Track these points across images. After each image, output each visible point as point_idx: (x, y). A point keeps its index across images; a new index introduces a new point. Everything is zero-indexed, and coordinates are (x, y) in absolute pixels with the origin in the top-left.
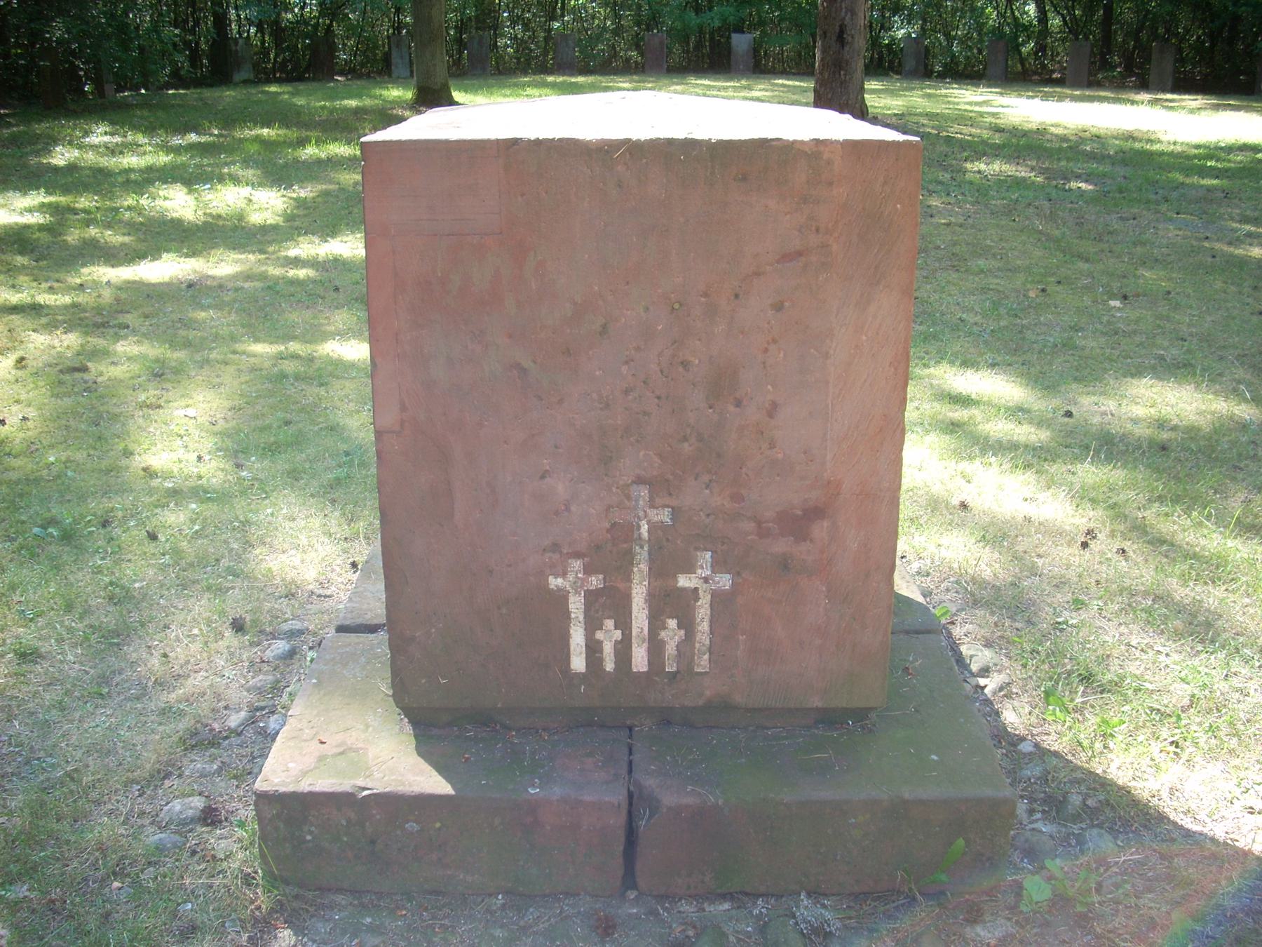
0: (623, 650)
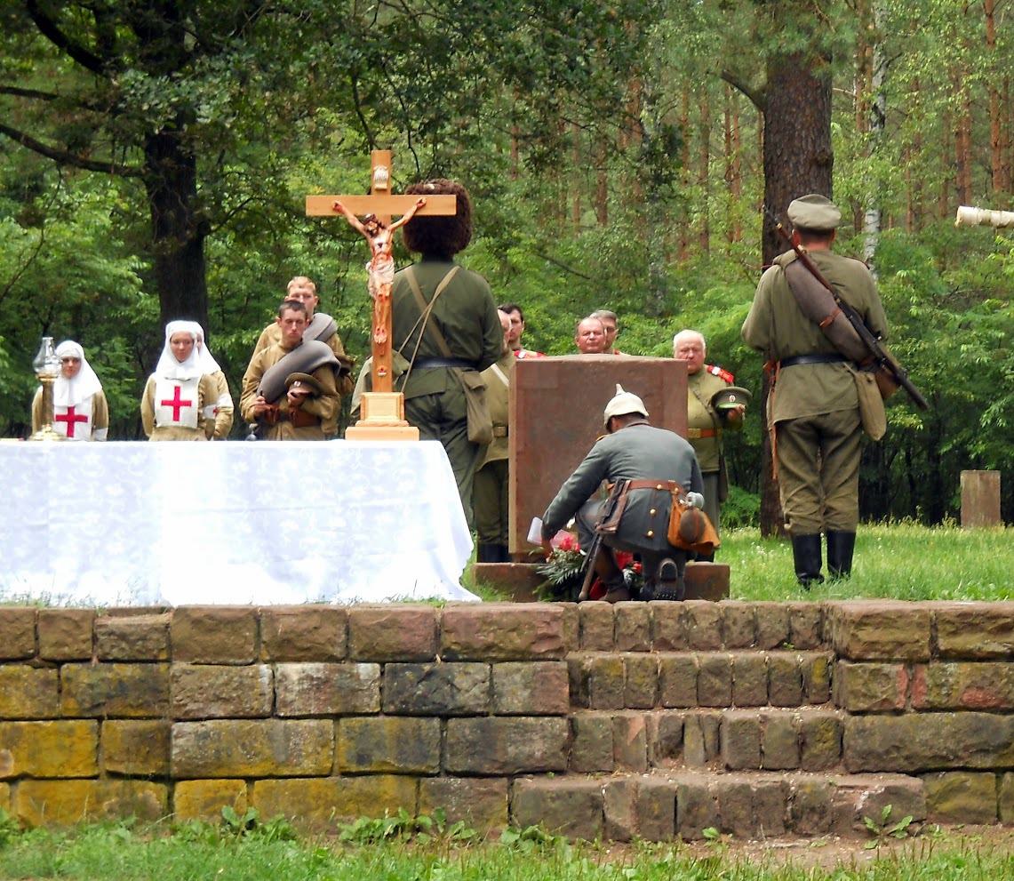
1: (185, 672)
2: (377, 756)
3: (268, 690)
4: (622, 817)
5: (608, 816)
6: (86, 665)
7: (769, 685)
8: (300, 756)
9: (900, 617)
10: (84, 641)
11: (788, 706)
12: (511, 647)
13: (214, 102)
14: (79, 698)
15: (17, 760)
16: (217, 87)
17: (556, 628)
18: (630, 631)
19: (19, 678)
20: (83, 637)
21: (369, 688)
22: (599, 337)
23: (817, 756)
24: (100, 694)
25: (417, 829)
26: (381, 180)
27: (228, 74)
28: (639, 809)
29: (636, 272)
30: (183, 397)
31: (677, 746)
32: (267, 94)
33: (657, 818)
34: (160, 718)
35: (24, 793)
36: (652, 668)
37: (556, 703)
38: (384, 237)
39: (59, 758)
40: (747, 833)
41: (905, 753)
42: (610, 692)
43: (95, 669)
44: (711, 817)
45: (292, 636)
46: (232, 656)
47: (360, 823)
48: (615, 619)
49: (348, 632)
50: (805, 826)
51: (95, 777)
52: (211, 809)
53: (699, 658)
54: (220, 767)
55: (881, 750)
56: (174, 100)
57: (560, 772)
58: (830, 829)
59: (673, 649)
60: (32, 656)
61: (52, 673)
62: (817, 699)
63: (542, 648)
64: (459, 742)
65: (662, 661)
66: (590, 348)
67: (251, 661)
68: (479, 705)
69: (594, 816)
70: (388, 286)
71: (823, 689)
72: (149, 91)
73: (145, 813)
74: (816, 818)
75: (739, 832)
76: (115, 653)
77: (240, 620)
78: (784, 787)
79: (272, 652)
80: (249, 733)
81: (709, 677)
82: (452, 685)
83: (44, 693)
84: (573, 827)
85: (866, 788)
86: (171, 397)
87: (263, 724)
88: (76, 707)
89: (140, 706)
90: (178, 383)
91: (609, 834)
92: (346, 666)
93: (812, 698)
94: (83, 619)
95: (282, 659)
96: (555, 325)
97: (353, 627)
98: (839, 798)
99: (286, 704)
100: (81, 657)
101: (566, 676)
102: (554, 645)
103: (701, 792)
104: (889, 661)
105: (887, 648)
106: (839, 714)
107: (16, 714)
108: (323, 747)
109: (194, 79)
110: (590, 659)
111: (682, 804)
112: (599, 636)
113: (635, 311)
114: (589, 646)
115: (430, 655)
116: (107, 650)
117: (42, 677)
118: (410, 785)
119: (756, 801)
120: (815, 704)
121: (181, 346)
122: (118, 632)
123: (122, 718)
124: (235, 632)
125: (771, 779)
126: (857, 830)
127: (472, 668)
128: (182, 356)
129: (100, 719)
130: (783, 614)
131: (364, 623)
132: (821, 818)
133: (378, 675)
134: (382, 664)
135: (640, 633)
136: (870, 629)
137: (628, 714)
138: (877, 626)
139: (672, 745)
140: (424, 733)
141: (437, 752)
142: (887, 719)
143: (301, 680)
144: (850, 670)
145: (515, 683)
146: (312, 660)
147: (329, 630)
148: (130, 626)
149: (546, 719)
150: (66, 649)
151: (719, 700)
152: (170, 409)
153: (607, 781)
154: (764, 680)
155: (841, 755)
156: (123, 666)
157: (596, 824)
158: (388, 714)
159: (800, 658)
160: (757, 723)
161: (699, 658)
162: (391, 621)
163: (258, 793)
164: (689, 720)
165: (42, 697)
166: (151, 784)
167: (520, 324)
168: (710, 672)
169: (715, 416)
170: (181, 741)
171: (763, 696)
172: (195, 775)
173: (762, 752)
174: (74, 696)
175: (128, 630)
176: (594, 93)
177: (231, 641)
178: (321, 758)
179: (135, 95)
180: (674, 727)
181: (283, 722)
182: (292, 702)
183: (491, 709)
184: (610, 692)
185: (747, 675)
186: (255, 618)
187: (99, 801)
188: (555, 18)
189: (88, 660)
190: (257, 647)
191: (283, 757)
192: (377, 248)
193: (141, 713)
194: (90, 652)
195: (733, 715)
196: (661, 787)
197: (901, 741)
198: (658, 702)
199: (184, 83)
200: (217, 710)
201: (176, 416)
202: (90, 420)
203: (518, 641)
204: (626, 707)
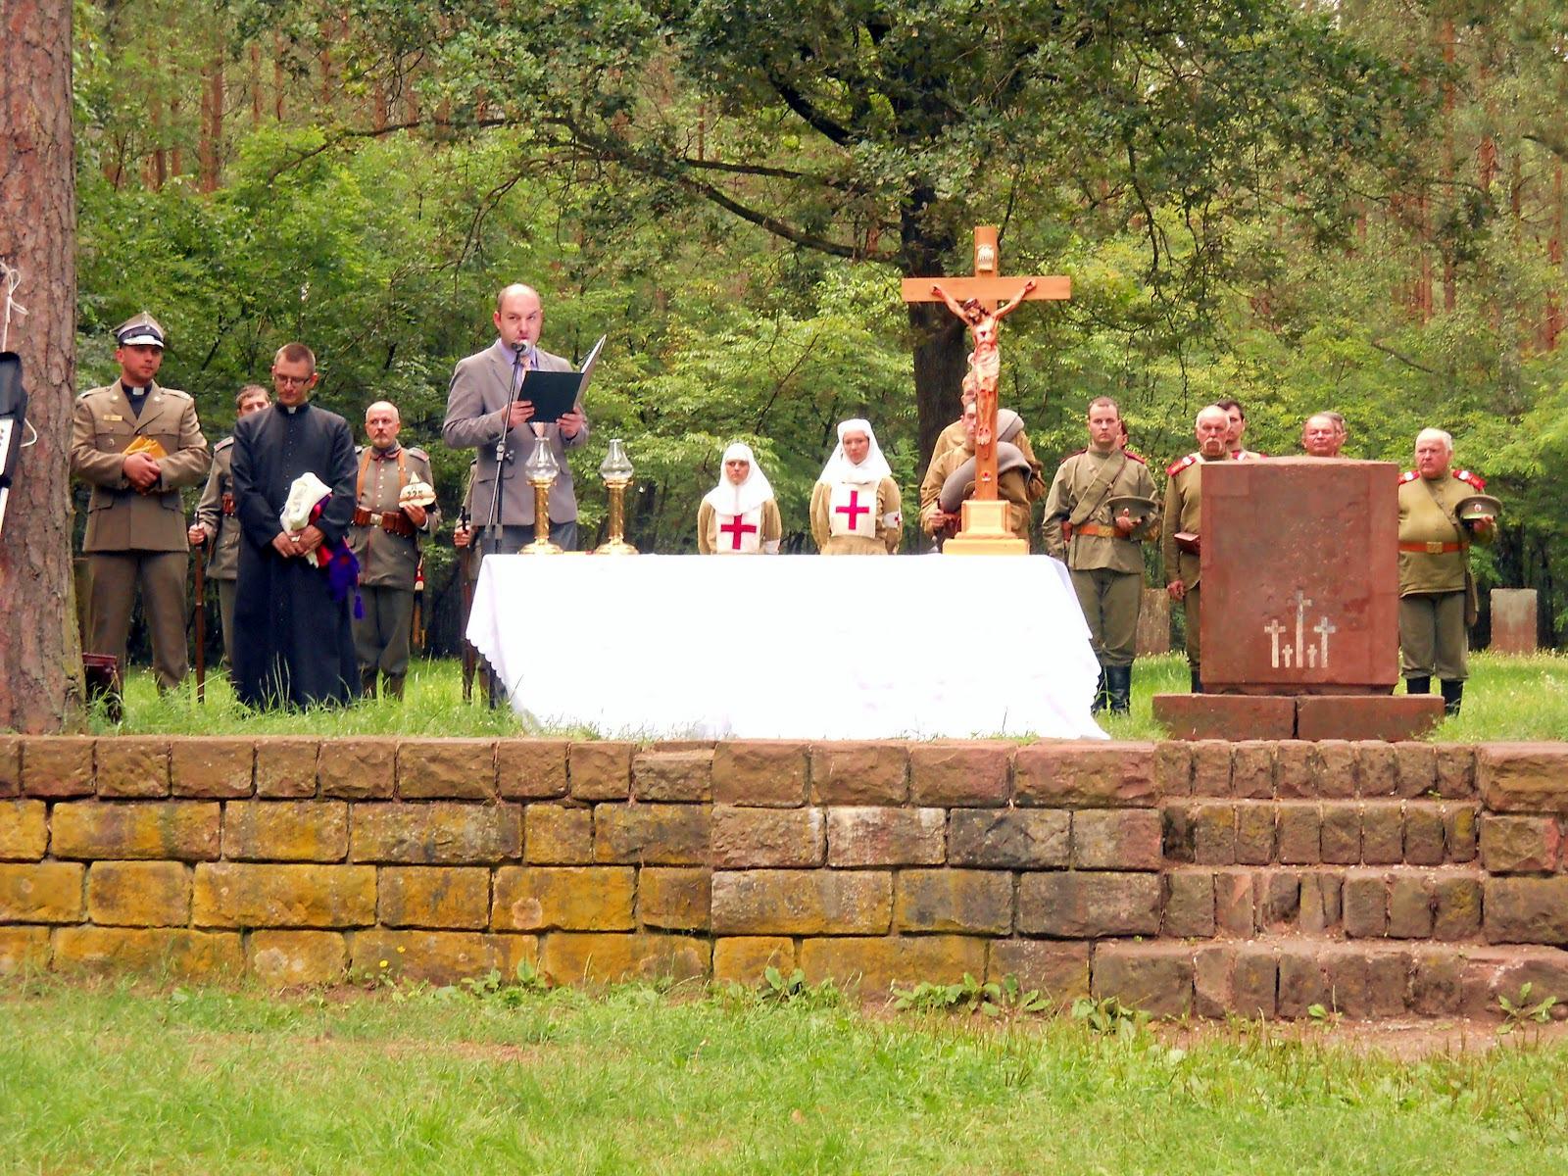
0: (1293, 657)
1: (725, 815)
2: (941, 914)
3: (818, 837)
4: (1211, 989)
5: (1198, 988)
6: (623, 804)
7: (1404, 840)
8: (854, 912)
9: (1549, 762)
10: (620, 779)
11: (1428, 864)
12: (1093, 792)
13: (954, 176)
14: (614, 842)
15: (546, 910)
16: (958, 159)
17: (1144, 771)
18: (1249, 775)
19: (548, 819)
20: (618, 774)
21: (932, 837)
22: (1328, 436)
23: (1451, 923)
24: (637, 838)
25: (986, 998)
26: (985, 261)
27: (971, 144)
28: (1236, 981)
29: (1486, 365)
30: (860, 504)
31: (1291, 909)
32: (1014, 166)
33: (1255, 991)
34: (699, 866)
35: (553, 947)
36: (1267, 818)
37: (1146, 856)
38: (988, 324)
39: (592, 909)
40: (1361, 1012)
41: (1555, 922)
42: (1218, 845)
43: (631, 811)
44: (1318, 992)
45: (845, 776)
46: (778, 798)
47: (920, 989)
48: (1233, 761)
49: (909, 773)
50: (1428, 1005)
51: (632, 931)
52: (753, 970)
53: (1325, 807)
54: (764, 923)
55: (1526, 918)
56: (911, 173)
57: (1149, 936)
58: (1458, 1010)
59: (1300, 796)
60: (563, 795)
61: (585, 814)
62: (1461, 856)
63: (1130, 794)
64: (1033, 900)
65: (1280, 809)
66: (1317, 449)
67: (799, 803)
68: (1056, 858)
69: (1181, 987)
70: (992, 381)
71: (1468, 846)
72: (883, 164)
73: (684, 971)
74: (1441, 996)
75: (1350, 1010)
76: (654, 793)
77: (787, 757)
78: (1405, 960)
79: (824, 794)
80: (796, 885)
81: (1334, 828)
82: (1027, 834)
83: (575, 835)
84: (1157, 1000)
85: (1500, 962)
86: (847, 503)
87: (812, 875)
88: (610, 851)
89: (681, 852)
90: (855, 488)
91: (1198, 1009)
92: (906, 811)
93: (1456, 856)
94: (619, 754)
95: (834, 802)
96: (1392, 424)
97: (914, 767)
98: (1470, 973)
99: (838, 853)
100: (617, 796)
101: (1157, 827)
102: (1145, 790)
103: (1306, 963)
104: (1536, 814)
105: (1534, 799)
106: (1482, 875)
107: (544, 860)
108: (880, 902)
109: (934, 151)
110: (1197, 806)
111: (1284, 977)
112: (1213, 780)
113: (1484, 408)
114: (1203, 791)
115: (1002, 800)
116: (645, 790)
117: (573, 818)
118: (977, 948)
119: (1369, 975)
120: (1458, 862)
121: (853, 446)
122: (657, 769)
123: (662, 865)
124: (781, 771)
125: (1397, 947)
126: (1490, 1011)
127: (1050, 815)
128: (857, 456)
129: (637, 866)
130: (1428, 757)
131: (926, 762)
132: (1448, 996)
133: (942, 821)
134: (948, 809)
135: (1262, 777)
136: (1513, 777)
137: (1236, 870)
138: (1522, 773)
139: (1286, 907)
140: (993, 888)
141: (1009, 911)
142: (1533, 882)
143: (855, 826)
144: (1490, 823)
145: (1099, 833)
146: (868, 803)
147: (886, 770)
148: (671, 762)
149: (1134, 875)
150: (600, 788)
151: (1345, 856)
152: (845, 517)
153: (1201, 947)
154: (1399, 834)
155: (1481, 922)
156: (663, 807)
157: (1184, 998)
158: (953, 866)
159: (1444, 808)
160: (1382, 883)
161: (1325, 807)
162: (960, 760)
163: (806, 953)
164: (1306, 879)
165: (573, 840)
166: (693, 940)
167: (1239, 422)
168: (1336, 824)
169: (1460, 527)
170: (720, 893)
171: (1397, 853)
172: (736, 931)
173: (1388, 918)
174: (608, 840)
175: (668, 767)
176: (1383, 158)
177: (778, 780)
178: (877, 915)
179: (868, 168)
180: (1289, 887)
181: (835, 874)
182: (845, 851)
183: (1072, 863)
184: (1218, 845)
185: (1379, 828)
186: (805, 754)
187: (635, 959)
188: (1343, 76)
189: (626, 800)
190: (807, 788)
191: (834, 913)
192: (980, 337)
193: (682, 860)
194: (626, 790)
195: (1355, 874)
196: (1260, 957)
197: (1550, 908)
198: (1274, 857)
199: (922, 155)
200: (760, 858)
201: (852, 525)
202: (758, 530)
203: (1102, 785)
204: (1237, 862)
